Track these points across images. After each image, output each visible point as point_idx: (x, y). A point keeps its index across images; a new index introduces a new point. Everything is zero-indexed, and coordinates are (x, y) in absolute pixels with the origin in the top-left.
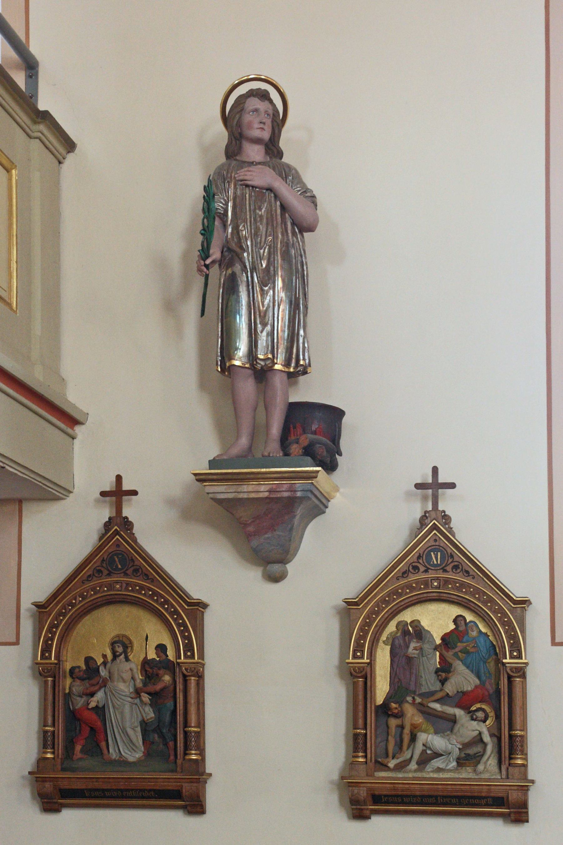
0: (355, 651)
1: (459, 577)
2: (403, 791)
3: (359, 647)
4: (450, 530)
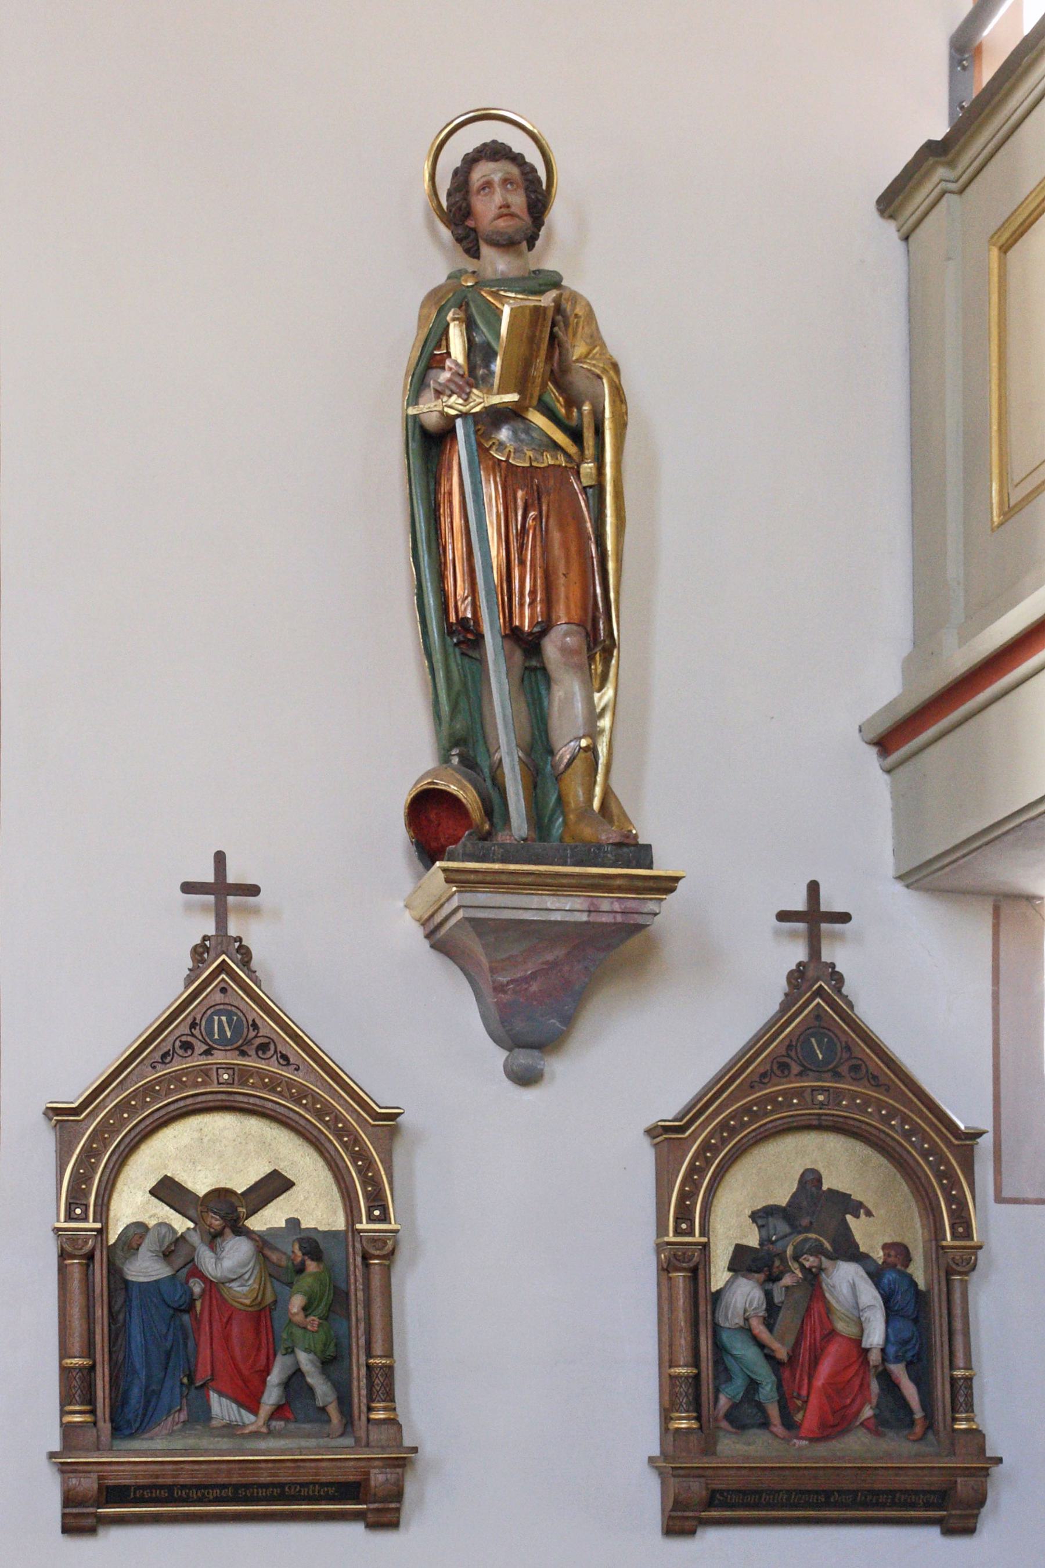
0: (677, 1220)
1: (272, 1067)
3: (684, 1214)
4: (251, 973)
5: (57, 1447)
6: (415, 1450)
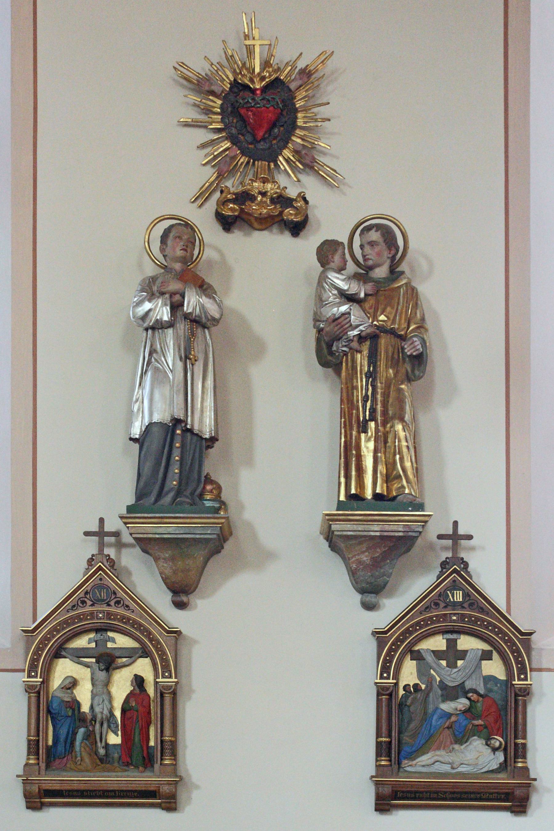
2: (463, 788)
5: (374, 774)
6: (535, 780)
